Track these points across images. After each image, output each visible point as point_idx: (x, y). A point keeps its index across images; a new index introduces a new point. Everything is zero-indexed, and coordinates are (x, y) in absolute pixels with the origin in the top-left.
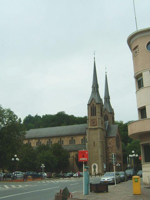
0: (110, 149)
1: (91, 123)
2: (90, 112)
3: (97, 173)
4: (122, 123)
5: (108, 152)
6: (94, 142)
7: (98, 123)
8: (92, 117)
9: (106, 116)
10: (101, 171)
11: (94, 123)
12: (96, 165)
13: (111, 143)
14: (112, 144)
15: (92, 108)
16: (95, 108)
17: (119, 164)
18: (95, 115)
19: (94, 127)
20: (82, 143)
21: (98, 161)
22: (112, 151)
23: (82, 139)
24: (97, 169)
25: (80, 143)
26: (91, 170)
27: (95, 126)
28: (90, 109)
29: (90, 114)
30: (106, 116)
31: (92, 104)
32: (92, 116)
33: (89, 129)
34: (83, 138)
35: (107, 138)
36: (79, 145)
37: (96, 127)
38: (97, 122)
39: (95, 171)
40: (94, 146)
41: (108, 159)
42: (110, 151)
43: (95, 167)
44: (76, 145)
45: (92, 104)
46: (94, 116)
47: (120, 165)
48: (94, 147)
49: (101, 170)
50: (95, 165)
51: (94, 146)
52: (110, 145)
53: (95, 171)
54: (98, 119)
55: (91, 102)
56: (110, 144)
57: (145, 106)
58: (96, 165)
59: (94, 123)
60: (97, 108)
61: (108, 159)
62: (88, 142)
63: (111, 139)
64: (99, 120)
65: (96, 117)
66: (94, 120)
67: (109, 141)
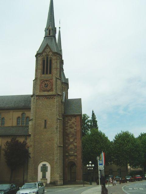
0: (70, 136)
1: (40, 85)
2: (40, 67)
3: (49, 182)
4: (46, 171)
5: (67, 141)
6: (45, 121)
7: (54, 87)
8: (43, 76)
9: (47, 58)
10: (57, 177)
11: (46, 86)
12: (48, 165)
13: (73, 125)
14: (75, 128)
15: (44, 61)
16: (51, 61)
17: (92, 164)
18: (50, 73)
19: (46, 93)
20: (17, 124)
21: (51, 157)
22: (74, 140)
23: (18, 118)
24: (48, 174)
25: (15, 124)
26: (37, 175)
27: (48, 91)
28: (40, 62)
29: (40, 71)
30: (47, 58)
31: (44, 54)
32: (43, 73)
33: (37, 96)
34: (20, 116)
35: (67, 116)
36: (12, 127)
37: (50, 93)
38: (52, 85)
39: (44, 177)
40: (45, 127)
41: (67, 154)
42: (71, 140)
43: (44, 169)
44: (7, 127)
45: (44, 54)
46: (47, 73)
47: (93, 165)
48: (45, 130)
49: (58, 176)
50: (44, 165)
51: (45, 127)
52: (72, 130)
53: (44, 177)
54: (54, 79)
55: (44, 51)
56: (72, 128)
57: (80, 99)
58: (48, 165)
59: (47, 86)
60: (53, 62)
61: (67, 154)
62: (34, 121)
63: (73, 120)
64: (56, 81)
65: (50, 75)
66: (47, 81)
67: (70, 122)
